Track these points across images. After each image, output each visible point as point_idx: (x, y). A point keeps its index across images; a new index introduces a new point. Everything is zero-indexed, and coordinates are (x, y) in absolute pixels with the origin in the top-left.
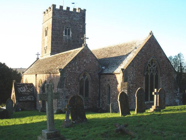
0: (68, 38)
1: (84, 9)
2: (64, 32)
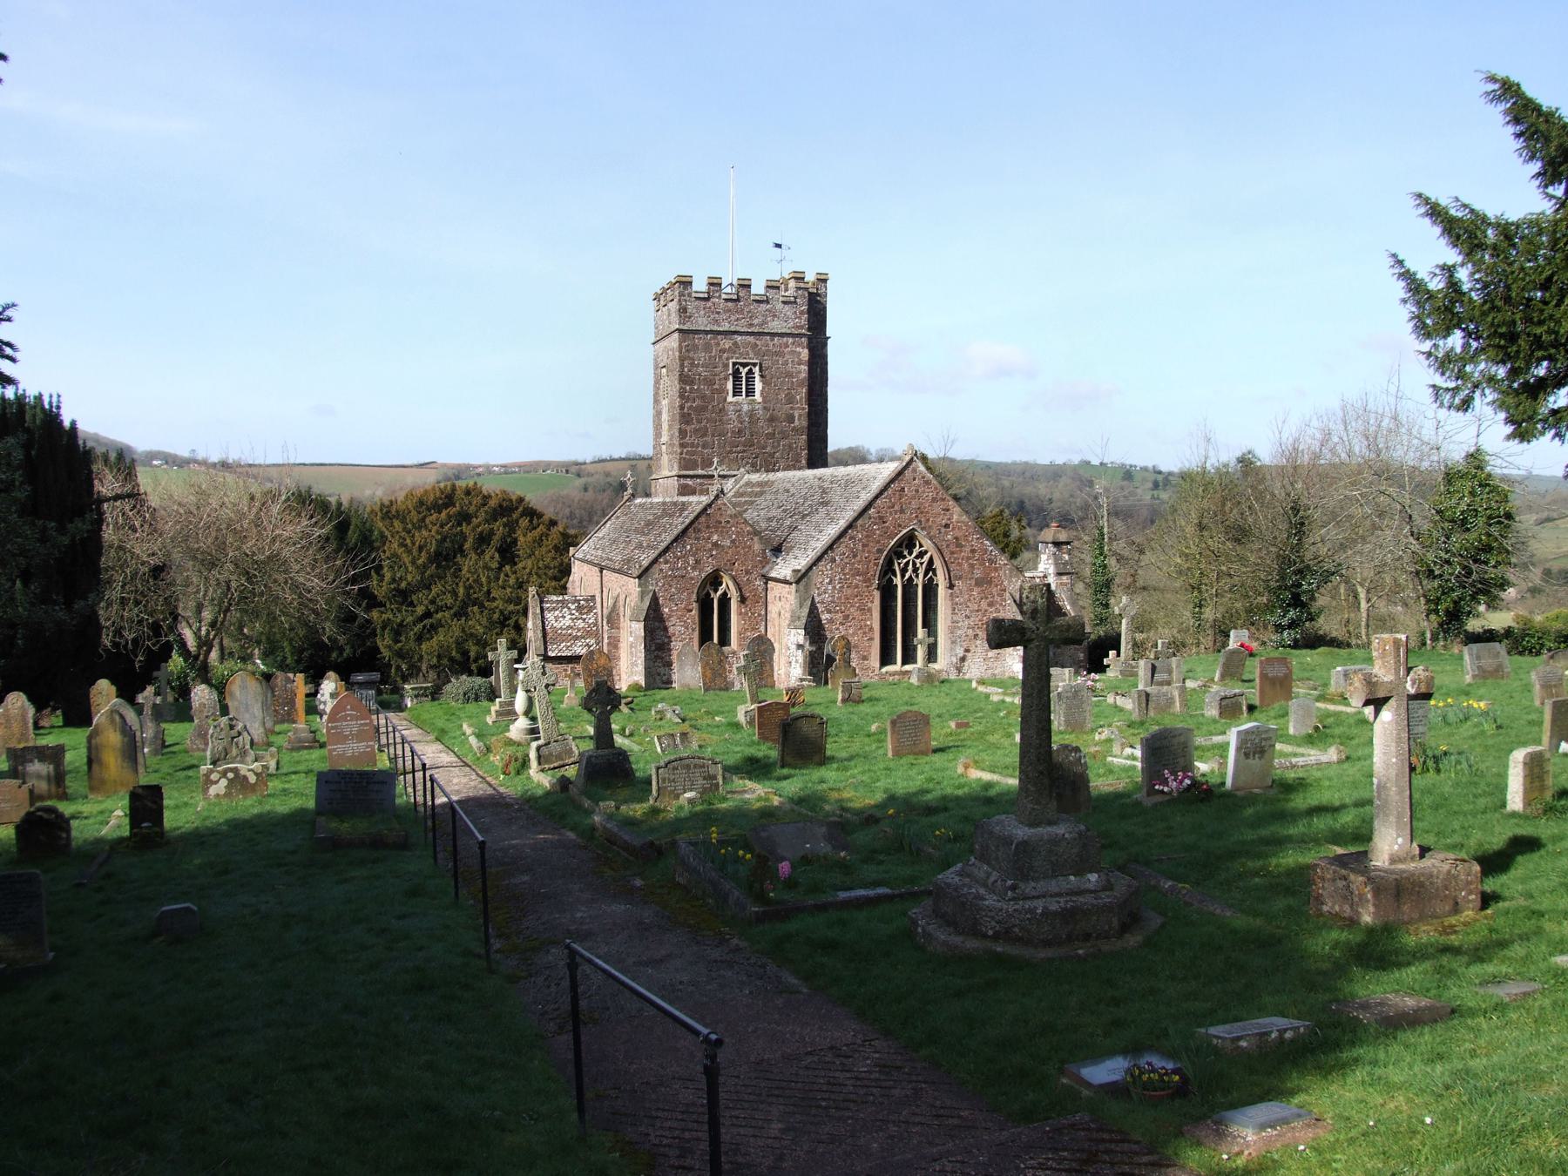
0: (746, 408)
2: (730, 386)
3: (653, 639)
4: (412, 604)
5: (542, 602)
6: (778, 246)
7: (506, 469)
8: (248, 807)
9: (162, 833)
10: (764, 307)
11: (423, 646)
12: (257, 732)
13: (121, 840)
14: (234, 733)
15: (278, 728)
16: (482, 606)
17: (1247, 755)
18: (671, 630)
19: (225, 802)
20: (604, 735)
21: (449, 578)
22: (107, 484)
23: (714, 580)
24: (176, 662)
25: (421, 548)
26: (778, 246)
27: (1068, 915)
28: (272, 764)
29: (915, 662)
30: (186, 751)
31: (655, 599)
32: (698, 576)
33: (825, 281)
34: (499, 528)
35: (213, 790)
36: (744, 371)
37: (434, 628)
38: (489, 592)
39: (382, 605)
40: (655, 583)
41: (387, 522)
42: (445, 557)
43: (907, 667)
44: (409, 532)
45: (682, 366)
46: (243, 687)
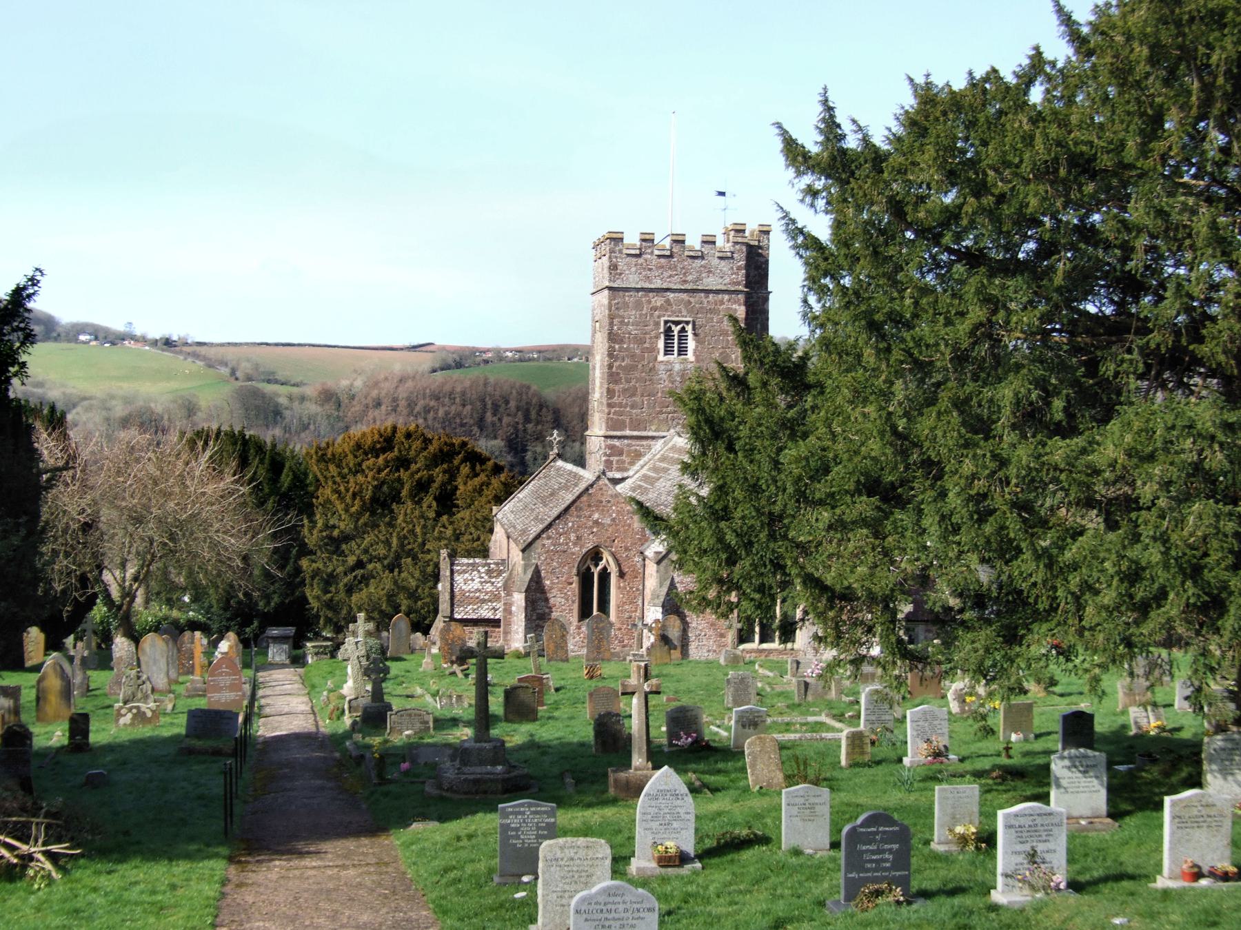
0: (677, 367)
1: (837, 164)
2: (661, 344)
3: (534, 610)
4: (342, 554)
5: (452, 564)
6: (722, 194)
7: (522, 355)
8: (145, 732)
9: (88, 744)
10: (698, 262)
11: (354, 598)
12: (161, 681)
13: (63, 747)
14: (140, 682)
15: (181, 679)
16: (415, 558)
17: (744, 726)
18: (552, 601)
19: (130, 729)
20: (378, 694)
21: (383, 528)
22: (46, 447)
23: (595, 555)
24: (99, 611)
25: (354, 495)
26: (722, 194)
27: (476, 782)
28: (170, 707)
29: (753, 641)
30: (106, 695)
31: (537, 572)
32: (579, 551)
33: (767, 233)
34: (439, 475)
35: (122, 721)
36: (676, 329)
37: (365, 580)
38: (424, 544)
39: (312, 553)
40: (538, 556)
41: (322, 465)
42: (381, 503)
43: (765, 646)
44: (344, 477)
45: (611, 324)
46: (153, 646)
